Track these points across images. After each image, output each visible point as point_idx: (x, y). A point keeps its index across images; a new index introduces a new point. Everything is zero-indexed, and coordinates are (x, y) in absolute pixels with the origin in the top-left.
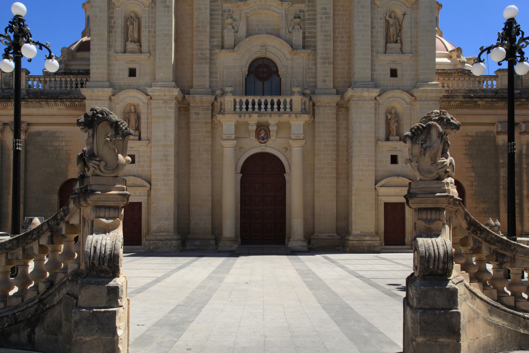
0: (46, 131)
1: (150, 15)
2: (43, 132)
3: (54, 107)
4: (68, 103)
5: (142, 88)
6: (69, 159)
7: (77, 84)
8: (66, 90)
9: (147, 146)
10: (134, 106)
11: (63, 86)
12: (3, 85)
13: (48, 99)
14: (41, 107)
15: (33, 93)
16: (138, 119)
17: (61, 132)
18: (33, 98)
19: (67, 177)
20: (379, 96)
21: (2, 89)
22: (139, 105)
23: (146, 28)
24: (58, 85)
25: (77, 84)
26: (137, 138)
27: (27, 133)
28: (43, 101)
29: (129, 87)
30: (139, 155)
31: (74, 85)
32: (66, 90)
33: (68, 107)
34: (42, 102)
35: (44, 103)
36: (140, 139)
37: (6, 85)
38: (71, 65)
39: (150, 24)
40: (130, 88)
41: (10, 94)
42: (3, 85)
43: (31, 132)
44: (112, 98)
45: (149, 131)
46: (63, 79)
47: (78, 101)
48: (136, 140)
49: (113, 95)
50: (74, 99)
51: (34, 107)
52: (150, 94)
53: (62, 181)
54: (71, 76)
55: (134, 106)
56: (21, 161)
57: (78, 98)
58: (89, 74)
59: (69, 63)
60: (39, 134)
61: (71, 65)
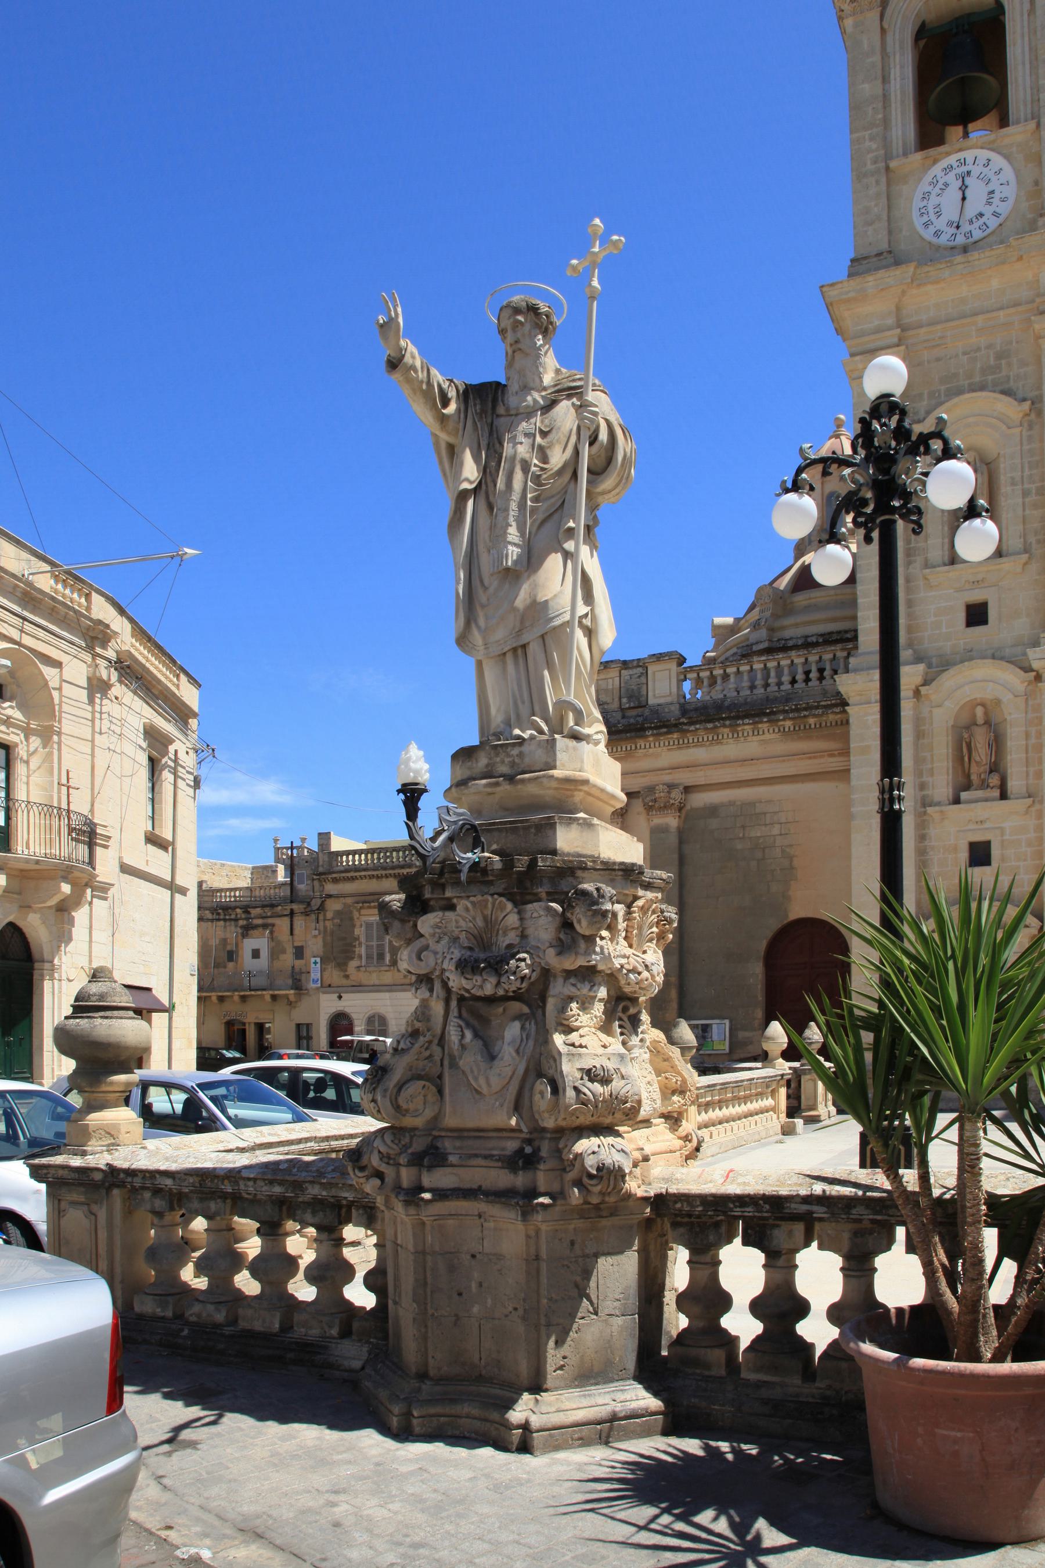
0: (732, 803)
1: (1026, 447)
2: (723, 805)
3: (750, 739)
4: (788, 724)
5: (1007, 652)
6: (792, 868)
7: (807, 673)
8: (779, 690)
9: (1027, 813)
10: (983, 705)
11: (797, 678)
12: (624, 700)
13: (738, 717)
14: (719, 742)
15: (696, 709)
16: (997, 743)
17: (769, 801)
18: (700, 722)
19: (787, 916)
20: (926, 683)
21: (622, 710)
22: (998, 702)
23: (1013, 483)
24: (746, 684)
25: (807, 673)
26: (996, 793)
27: (684, 812)
28: (724, 726)
29: (969, 655)
30: (1003, 841)
31: (800, 677)
32: (779, 690)
33: (785, 733)
34: (722, 730)
35: (726, 730)
36: (1004, 796)
37: (630, 698)
38: (783, 628)
39: (1027, 472)
40: (971, 659)
41: (640, 719)
42: (624, 700)
43: (692, 809)
44: (924, 690)
45: (1032, 770)
46: (771, 665)
47: (815, 716)
48: (993, 800)
49: (926, 683)
50: (805, 709)
51: (699, 744)
52: (1035, 665)
53: (773, 925)
54: (793, 653)
55: (983, 705)
56: (905, 882)
57: (817, 708)
58: (855, 638)
59: (777, 624)
60: (713, 811)
61: (783, 628)
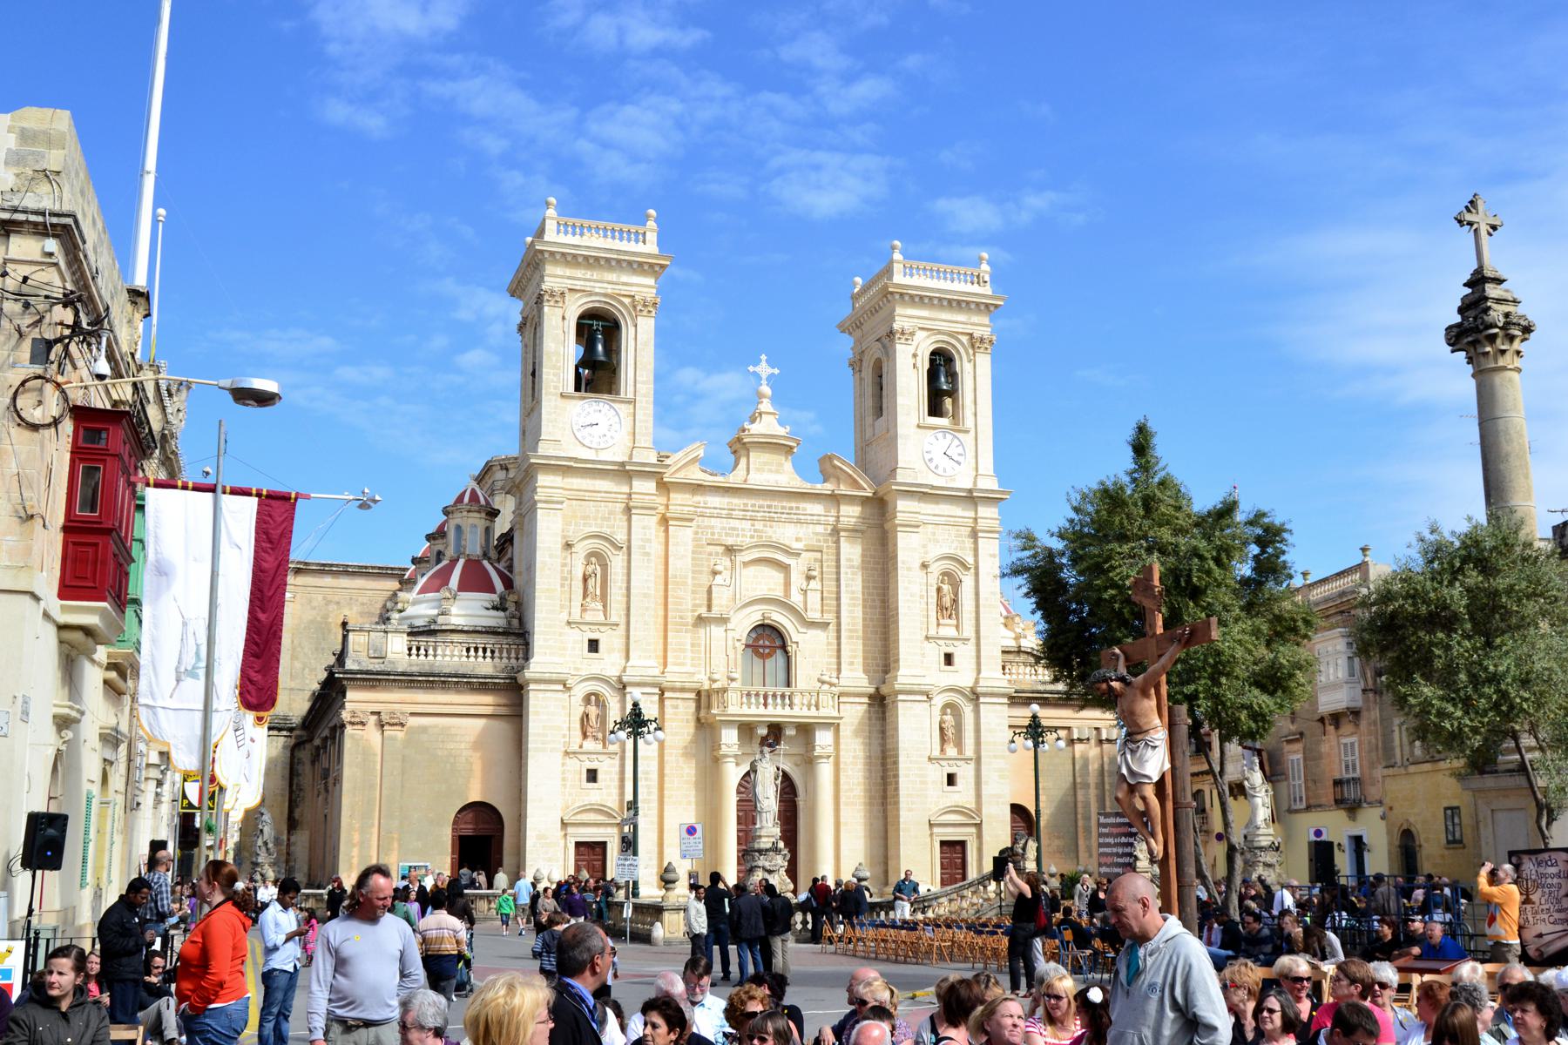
60: (424, 729)
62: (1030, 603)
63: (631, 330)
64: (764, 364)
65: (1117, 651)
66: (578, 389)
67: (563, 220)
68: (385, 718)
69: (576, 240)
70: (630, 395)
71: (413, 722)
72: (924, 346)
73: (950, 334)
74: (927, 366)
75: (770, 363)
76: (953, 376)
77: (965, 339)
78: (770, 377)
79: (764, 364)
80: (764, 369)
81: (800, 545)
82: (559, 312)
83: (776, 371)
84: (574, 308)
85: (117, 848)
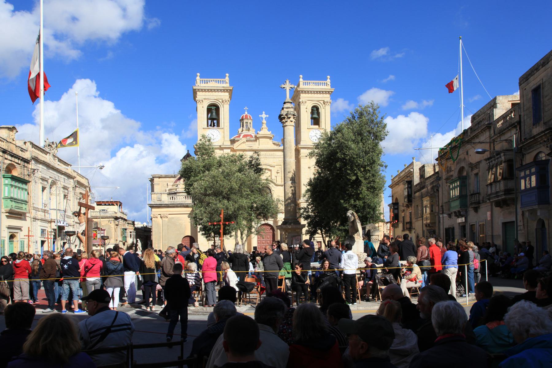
60: (173, 218)
62: (71, 91)
63: (222, 108)
64: (264, 114)
65: (417, 194)
66: (208, 126)
67: (304, 81)
68: (162, 216)
69: (206, 85)
70: (223, 127)
71: (170, 216)
72: (309, 105)
73: (318, 101)
74: (310, 111)
75: (266, 114)
76: (318, 114)
77: (322, 102)
78: (265, 118)
79: (264, 114)
80: (264, 116)
81: (275, 164)
82: (202, 106)
83: (264, 112)
84: (206, 104)
85: (130, 360)
